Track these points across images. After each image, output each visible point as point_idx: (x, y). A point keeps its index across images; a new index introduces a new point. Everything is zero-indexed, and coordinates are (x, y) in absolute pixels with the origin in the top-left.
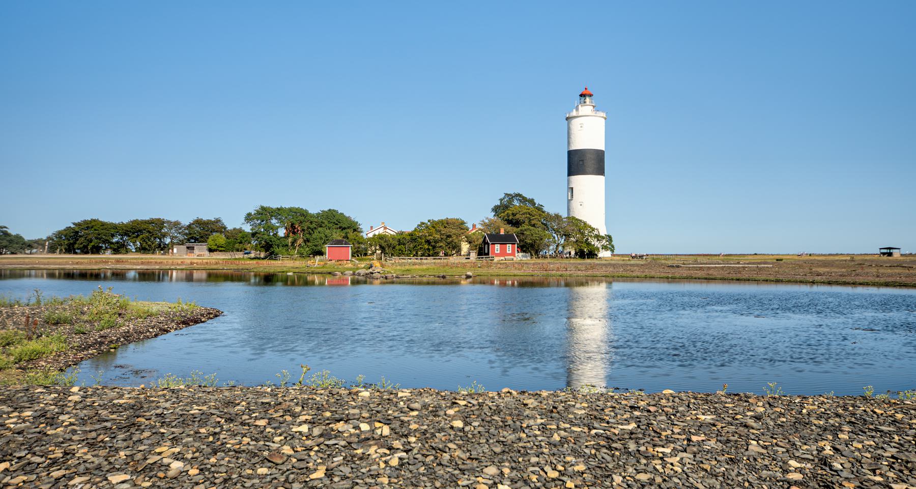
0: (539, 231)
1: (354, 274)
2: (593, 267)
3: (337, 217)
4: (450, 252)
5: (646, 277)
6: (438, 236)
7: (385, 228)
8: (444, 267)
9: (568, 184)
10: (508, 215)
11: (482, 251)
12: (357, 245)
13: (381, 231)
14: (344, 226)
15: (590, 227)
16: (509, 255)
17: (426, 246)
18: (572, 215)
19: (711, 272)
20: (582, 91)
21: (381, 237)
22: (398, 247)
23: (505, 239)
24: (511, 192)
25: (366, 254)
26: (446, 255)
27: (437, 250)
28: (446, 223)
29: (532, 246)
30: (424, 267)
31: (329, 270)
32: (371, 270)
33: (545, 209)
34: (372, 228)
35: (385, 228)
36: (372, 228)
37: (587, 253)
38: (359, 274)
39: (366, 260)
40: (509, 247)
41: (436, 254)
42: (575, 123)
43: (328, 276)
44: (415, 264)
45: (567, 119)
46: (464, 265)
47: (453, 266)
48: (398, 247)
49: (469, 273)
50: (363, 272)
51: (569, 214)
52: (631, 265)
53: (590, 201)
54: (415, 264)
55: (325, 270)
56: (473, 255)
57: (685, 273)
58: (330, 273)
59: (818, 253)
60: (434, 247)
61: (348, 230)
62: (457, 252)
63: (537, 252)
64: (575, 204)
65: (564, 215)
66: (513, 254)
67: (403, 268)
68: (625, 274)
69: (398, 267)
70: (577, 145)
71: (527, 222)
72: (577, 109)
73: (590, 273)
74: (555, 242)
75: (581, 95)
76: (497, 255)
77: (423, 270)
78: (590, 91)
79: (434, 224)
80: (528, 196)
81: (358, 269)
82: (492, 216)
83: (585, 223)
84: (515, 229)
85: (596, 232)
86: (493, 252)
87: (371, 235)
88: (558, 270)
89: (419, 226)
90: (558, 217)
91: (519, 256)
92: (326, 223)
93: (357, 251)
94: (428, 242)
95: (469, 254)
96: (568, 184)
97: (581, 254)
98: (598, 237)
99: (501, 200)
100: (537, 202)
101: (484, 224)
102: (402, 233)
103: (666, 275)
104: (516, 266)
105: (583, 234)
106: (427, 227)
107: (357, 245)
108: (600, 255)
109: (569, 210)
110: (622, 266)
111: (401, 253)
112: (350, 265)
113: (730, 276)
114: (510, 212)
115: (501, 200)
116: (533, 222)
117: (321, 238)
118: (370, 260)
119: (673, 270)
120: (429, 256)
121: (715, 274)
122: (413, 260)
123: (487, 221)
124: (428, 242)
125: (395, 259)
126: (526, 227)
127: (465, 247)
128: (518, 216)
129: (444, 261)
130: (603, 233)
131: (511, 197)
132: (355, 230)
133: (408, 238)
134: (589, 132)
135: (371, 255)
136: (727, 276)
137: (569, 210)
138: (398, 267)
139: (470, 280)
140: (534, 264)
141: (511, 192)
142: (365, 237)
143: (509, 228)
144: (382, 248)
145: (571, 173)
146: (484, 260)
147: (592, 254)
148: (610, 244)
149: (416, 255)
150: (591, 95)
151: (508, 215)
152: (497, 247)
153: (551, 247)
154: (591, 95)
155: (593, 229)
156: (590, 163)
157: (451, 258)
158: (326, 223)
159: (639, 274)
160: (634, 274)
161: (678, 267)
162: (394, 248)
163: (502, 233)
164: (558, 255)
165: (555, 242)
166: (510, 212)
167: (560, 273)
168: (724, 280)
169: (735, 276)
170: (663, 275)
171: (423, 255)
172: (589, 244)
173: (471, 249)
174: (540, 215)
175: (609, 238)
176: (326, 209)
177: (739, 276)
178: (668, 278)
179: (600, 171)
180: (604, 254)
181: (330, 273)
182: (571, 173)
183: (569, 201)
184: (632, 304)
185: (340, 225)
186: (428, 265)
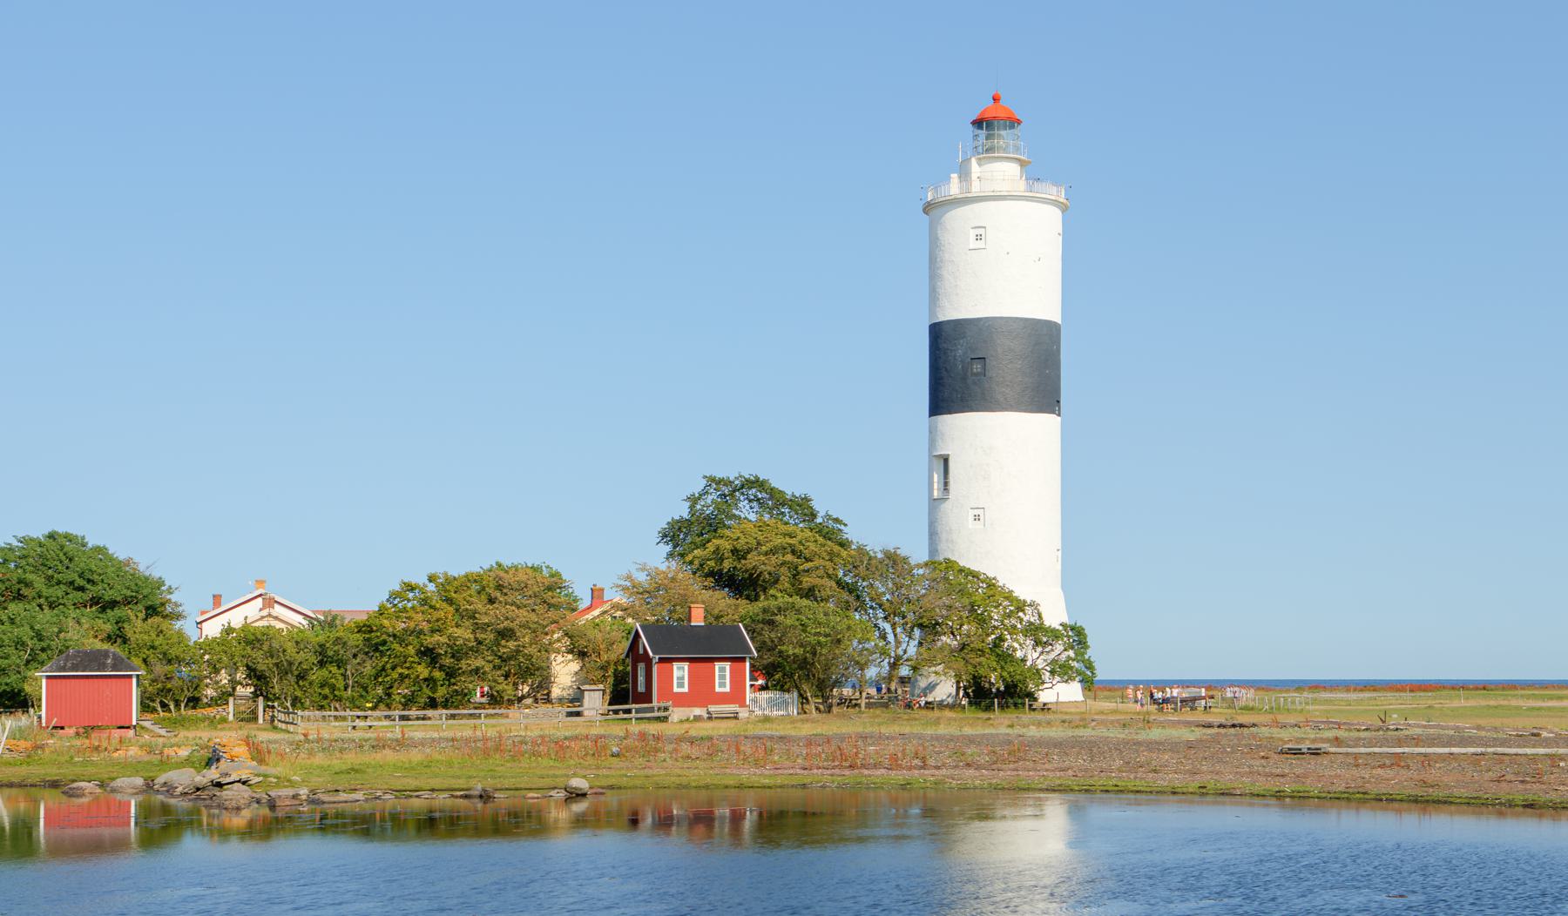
0: (827, 613)
1: (149, 786)
2: (1018, 751)
3: (81, 563)
4: (507, 689)
5: (1203, 792)
6: (464, 634)
7: (270, 602)
8: (486, 753)
9: (932, 442)
10: (718, 556)
11: (626, 691)
12: (160, 669)
13: (252, 611)
14: (109, 595)
15: (1009, 596)
17: (423, 671)
18: (945, 553)
19: (1433, 774)
21: (252, 639)
22: (317, 675)
23: (705, 646)
24: (730, 472)
25: (194, 702)
26: (495, 700)
27: (464, 682)
28: (496, 586)
29: (804, 664)
30: (416, 756)
31: (53, 773)
32: (213, 774)
33: (852, 533)
34: (217, 600)
35: (270, 602)
36: (217, 600)
37: (998, 691)
38: (169, 789)
39: (195, 722)
40: (722, 675)
41: (455, 701)
42: (958, 222)
43: (48, 793)
44: (379, 745)
45: (928, 208)
46: (560, 747)
47: (517, 750)
48: (317, 675)
49: (578, 783)
50: (184, 778)
51: (933, 550)
52: (1153, 746)
53: (1009, 507)
54: (379, 745)
55: (35, 772)
56: (595, 701)
57: (1340, 777)
58: (54, 785)
60: (451, 674)
61: (127, 612)
62: (535, 689)
63: (823, 687)
64: (956, 514)
65: (917, 553)
67: (337, 763)
68: (1128, 780)
69: (319, 759)
70: (961, 306)
71: (785, 583)
72: (965, 174)
73: (1005, 776)
74: (884, 653)
75: (978, 123)
76: (681, 700)
77: (410, 769)
79: (450, 590)
80: (790, 487)
81: (165, 764)
82: (658, 557)
83: (991, 584)
84: (745, 607)
85: (1028, 616)
86: (667, 692)
87: (213, 629)
88: (894, 763)
89: (393, 595)
90: (894, 560)
91: (760, 704)
92: (39, 582)
93: (165, 691)
94: (429, 654)
95: (577, 699)
96: (932, 442)
97: (979, 695)
98: (1039, 634)
99: (693, 500)
100: (821, 507)
101: (634, 589)
102: (331, 622)
103: (1273, 785)
104: (747, 748)
105: (982, 621)
106: (425, 602)
107: (160, 669)
108: (1045, 696)
109: (933, 534)
110: (1119, 747)
111: (328, 698)
112: (133, 751)
113: (1504, 792)
114: (726, 546)
115: (693, 500)
116: (807, 581)
117: (19, 644)
118: (212, 722)
119: (1297, 766)
120: (433, 704)
121: (1449, 781)
122: (382, 725)
123: (641, 577)
124: (429, 654)
125: (310, 724)
126: (783, 599)
127: (564, 672)
128: (753, 560)
129: (489, 725)
130: (1055, 616)
131: (731, 490)
132: (152, 611)
133: (356, 639)
134: (1010, 256)
135: (214, 702)
136: (1492, 790)
137: (933, 534)
138: (319, 759)
139: (580, 807)
140: (809, 741)
141: (731, 471)
142: (193, 635)
143: (722, 600)
144: (255, 675)
145: (939, 406)
146: (634, 726)
147: (1015, 694)
148: (1080, 656)
149: (385, 701)
151: (718, 556)
152: (681, 671)
153: (871, 672)
155: (1021, 606)
156: (1007, 367)
157: (514, 713)
158: (39, 582)
159: (1177, 780)
160: (1162, 782)
161: (1316, 753)
162: (301, 677)
163: (698, 620)
164: (897, 694)
165: (884, 653)
166: (726, 546)
167: (898, 776)
168: (1477, 805)
169: (1518, 793)
170: (1261, 785)
171: (408, 702)
172: (1005, 658)
173: (584, 678)
174: (832, 556)
175: (1077, 637)
176: (39, 533)
177: (1535, 792)
178: (1279, 796)
179: (1045, 397)
180: (1061, 693)
181: (54, 785)
182: (939, 406)
183: (935, 504)
184: (1115, 712)
185: (93, 591)
186: (419, 750)
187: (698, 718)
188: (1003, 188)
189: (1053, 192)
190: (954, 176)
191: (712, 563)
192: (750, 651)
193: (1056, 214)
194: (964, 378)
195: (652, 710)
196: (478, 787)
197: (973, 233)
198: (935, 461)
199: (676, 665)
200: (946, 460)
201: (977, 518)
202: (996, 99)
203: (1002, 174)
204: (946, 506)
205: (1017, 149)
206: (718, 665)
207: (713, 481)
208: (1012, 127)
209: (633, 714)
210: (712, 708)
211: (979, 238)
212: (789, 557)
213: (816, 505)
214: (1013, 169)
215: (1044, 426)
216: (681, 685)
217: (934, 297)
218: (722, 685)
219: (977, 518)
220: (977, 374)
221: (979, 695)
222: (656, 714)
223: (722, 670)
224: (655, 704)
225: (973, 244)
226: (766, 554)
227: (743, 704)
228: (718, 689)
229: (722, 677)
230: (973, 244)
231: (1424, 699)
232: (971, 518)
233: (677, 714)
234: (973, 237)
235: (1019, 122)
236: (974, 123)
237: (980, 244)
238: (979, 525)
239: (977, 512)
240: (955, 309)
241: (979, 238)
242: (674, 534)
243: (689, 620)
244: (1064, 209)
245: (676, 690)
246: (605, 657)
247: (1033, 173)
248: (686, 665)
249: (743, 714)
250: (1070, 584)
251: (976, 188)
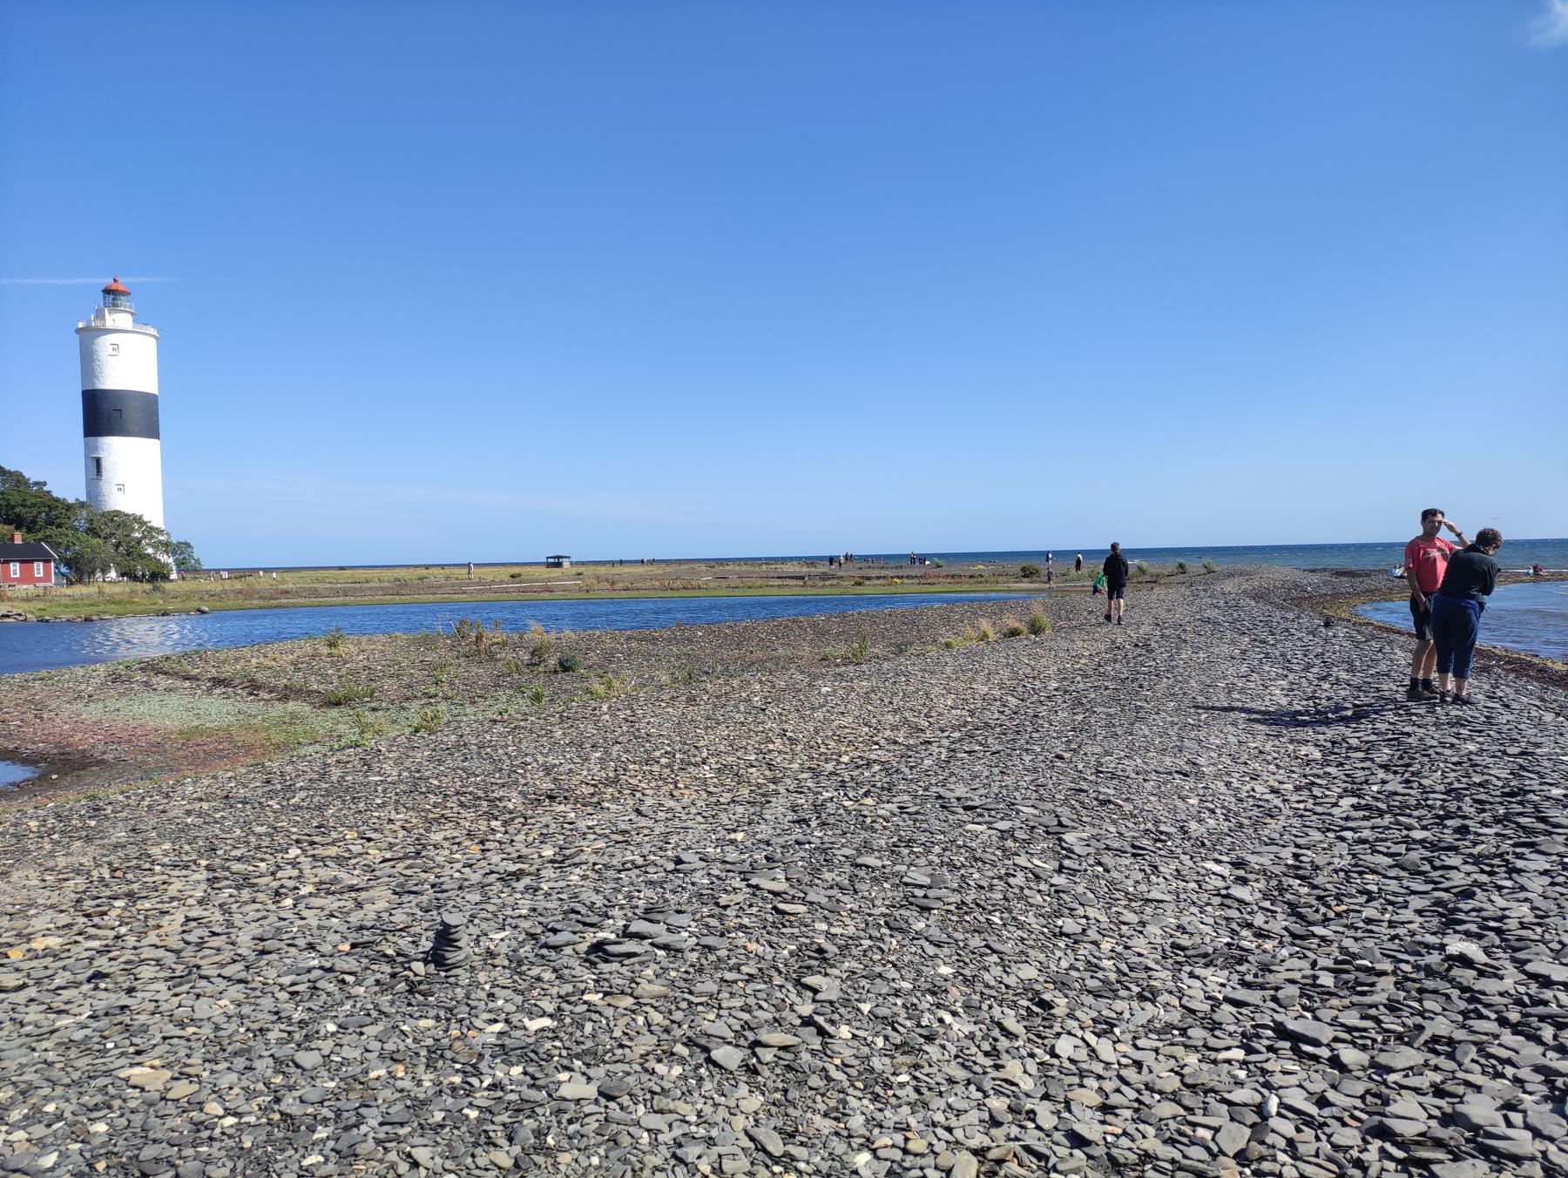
40: (38, 569)
42: (104, 344)
53: (135, 479)
76: (20, 581)
98: (167, 547)
134: (130, 362)
156: (133, 414)
189: (152, 331)
203: (119, 319)
215: (153, 444)
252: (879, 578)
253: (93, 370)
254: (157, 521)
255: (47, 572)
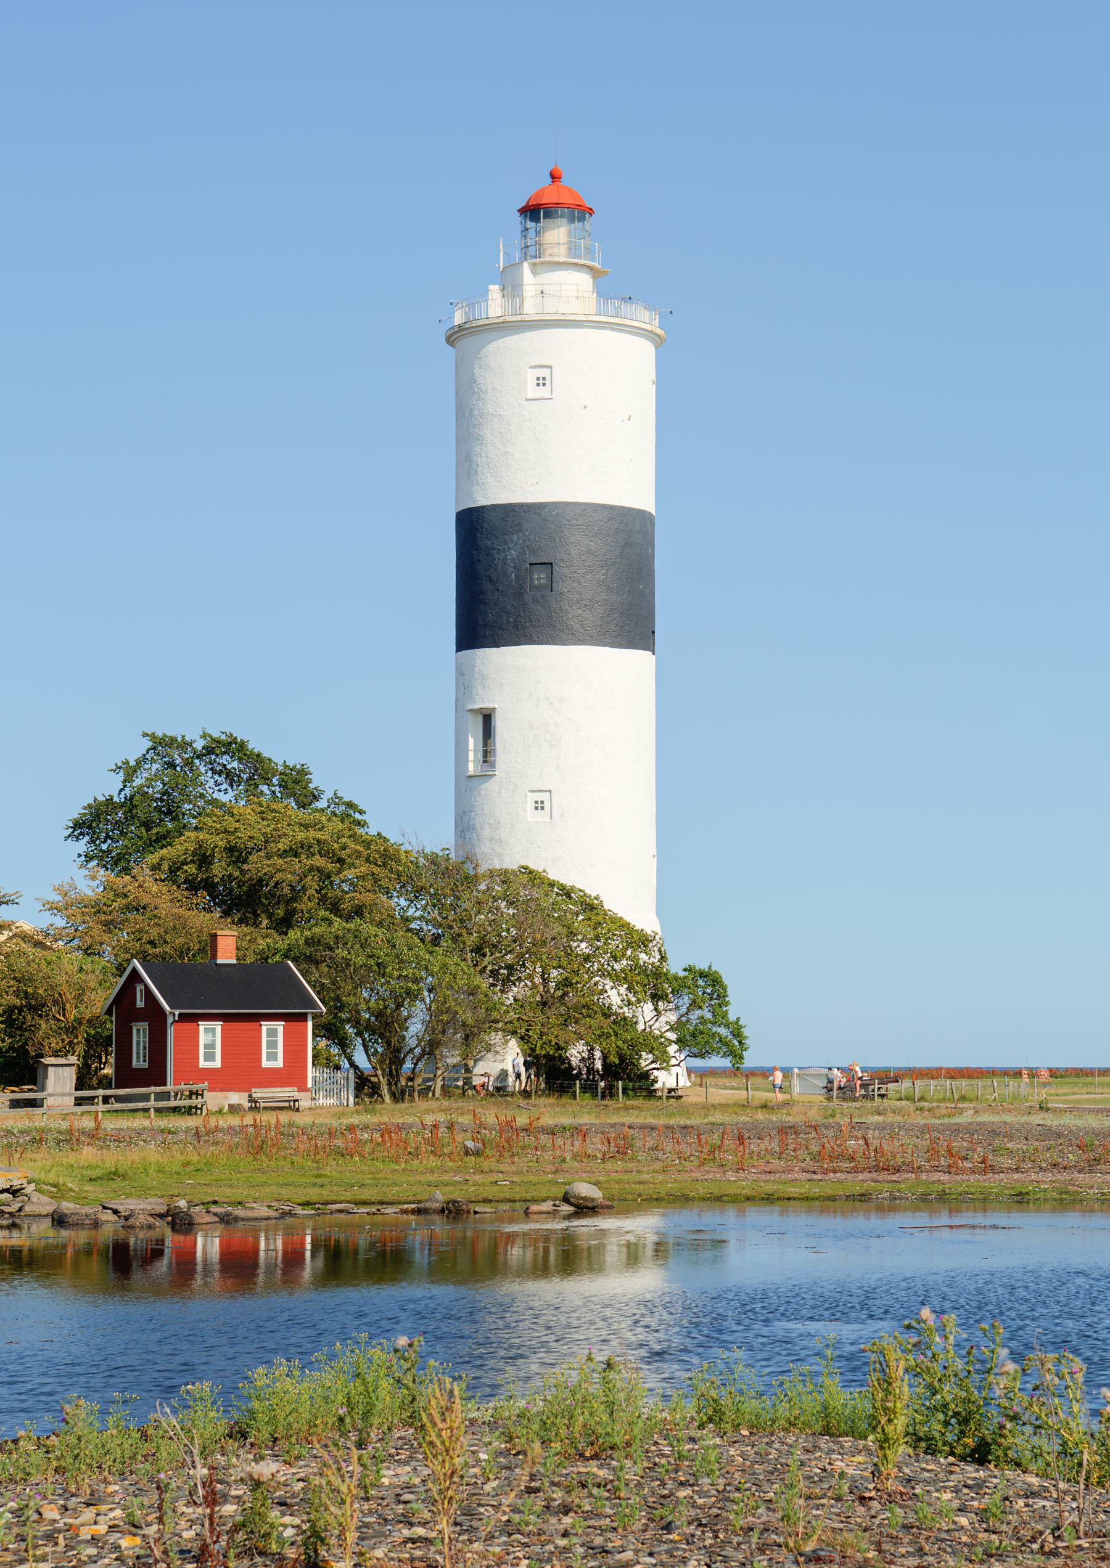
16: (274, 1078)
20: (532, 185)
23: (247, 997)
40: (272, 1040)
42: (508, 362)
45: (455, 336)
53: (581, 781)
59: (1042, 1061)
66: (292, 1075)
72: (512, 288)
76: (220, 1080)
78: (579, 183)
97: (553, 1074)
98: (655, 985)
99: (129, 771)
128: (257, 865)
134: (582, 417)
147: (624, 1076)
150: (580, 212)
152: (210, 1036)
154: (580, 212)
156: (582, 580)
163: (226, 956)
183: (466, 787)
187: (234, 1109)
188: (555, 308)
189: (645, 318)
190: (494, 289)
191: (191, 869)
192: (314, 1006)
193: (646, 350)
194: (519, 594)
195: (165, 1096)
196: (440, 1196)
197: (531, 376)
198: (470, 717)
199: (203, 1026)
200: (488, 718)
201: (539, 806)
202: (554, 177)
203: (560, 286)
204: (490, 787)
205: (589, 252)
206: (266, 1026)
207: (161, 744)
208: (582, 219)
209: (152, 1103)
210: (257, 1093)
211: (541, 382)
212: (318, 861)
213: (316, 781)
214: (583, 281)
215: (636, 663)
216: (210, 1057)
217: (466, 466)
218: (272, 1056)
219: (539, 806)
220: (538, 588)
221: (553, 1074)
222: (173, 1103)
223: (272, 1033)
224: (170, 1087)
225: (532, 391)
226: (283, 854)
227: (303, 1088)
228: (265, 1064)
229: (272, 1045)
230: (532, 391)
231: (963, 1085)
232: (530, 805)
233: (213, 1100)
234: (531, 381)
235: (591, 211)
236: (523, 211)
237: (543, 392)
238: (542, 816)
239: (539, 797)
240: (494, 492)
241: (541, 382)
242: (89, 824)
243: (214, 955)
244: (659, 342)
245: (203, 1064)
246: (72, 1014)
247: (613, 289)
248: (218, 1026)
249: (305, 1103)
250: (661, 912)
251: (531, 308)
252: (20, 1394)
253: (473, 381)
254: (630, 895)
255: (294, 1052)
